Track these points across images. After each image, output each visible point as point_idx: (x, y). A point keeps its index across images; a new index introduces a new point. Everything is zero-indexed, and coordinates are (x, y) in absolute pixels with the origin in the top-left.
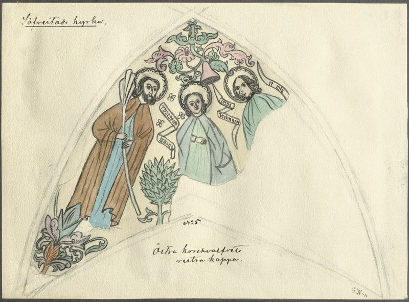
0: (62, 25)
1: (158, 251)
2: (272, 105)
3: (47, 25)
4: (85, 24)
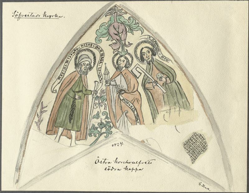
0: (36, 17)
1: (98, 162)
2: (185, 106)
3: (28, 17)
4: (51, 17)
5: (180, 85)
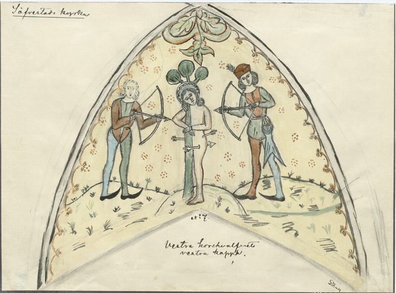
3: (37, 15)
5: (40, 260)
